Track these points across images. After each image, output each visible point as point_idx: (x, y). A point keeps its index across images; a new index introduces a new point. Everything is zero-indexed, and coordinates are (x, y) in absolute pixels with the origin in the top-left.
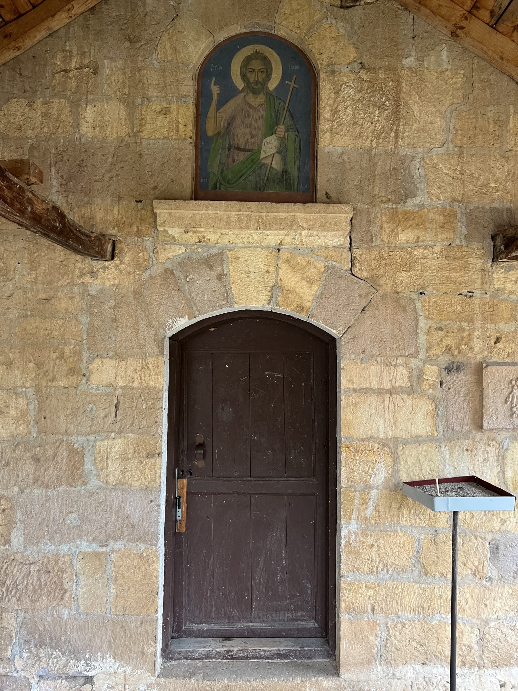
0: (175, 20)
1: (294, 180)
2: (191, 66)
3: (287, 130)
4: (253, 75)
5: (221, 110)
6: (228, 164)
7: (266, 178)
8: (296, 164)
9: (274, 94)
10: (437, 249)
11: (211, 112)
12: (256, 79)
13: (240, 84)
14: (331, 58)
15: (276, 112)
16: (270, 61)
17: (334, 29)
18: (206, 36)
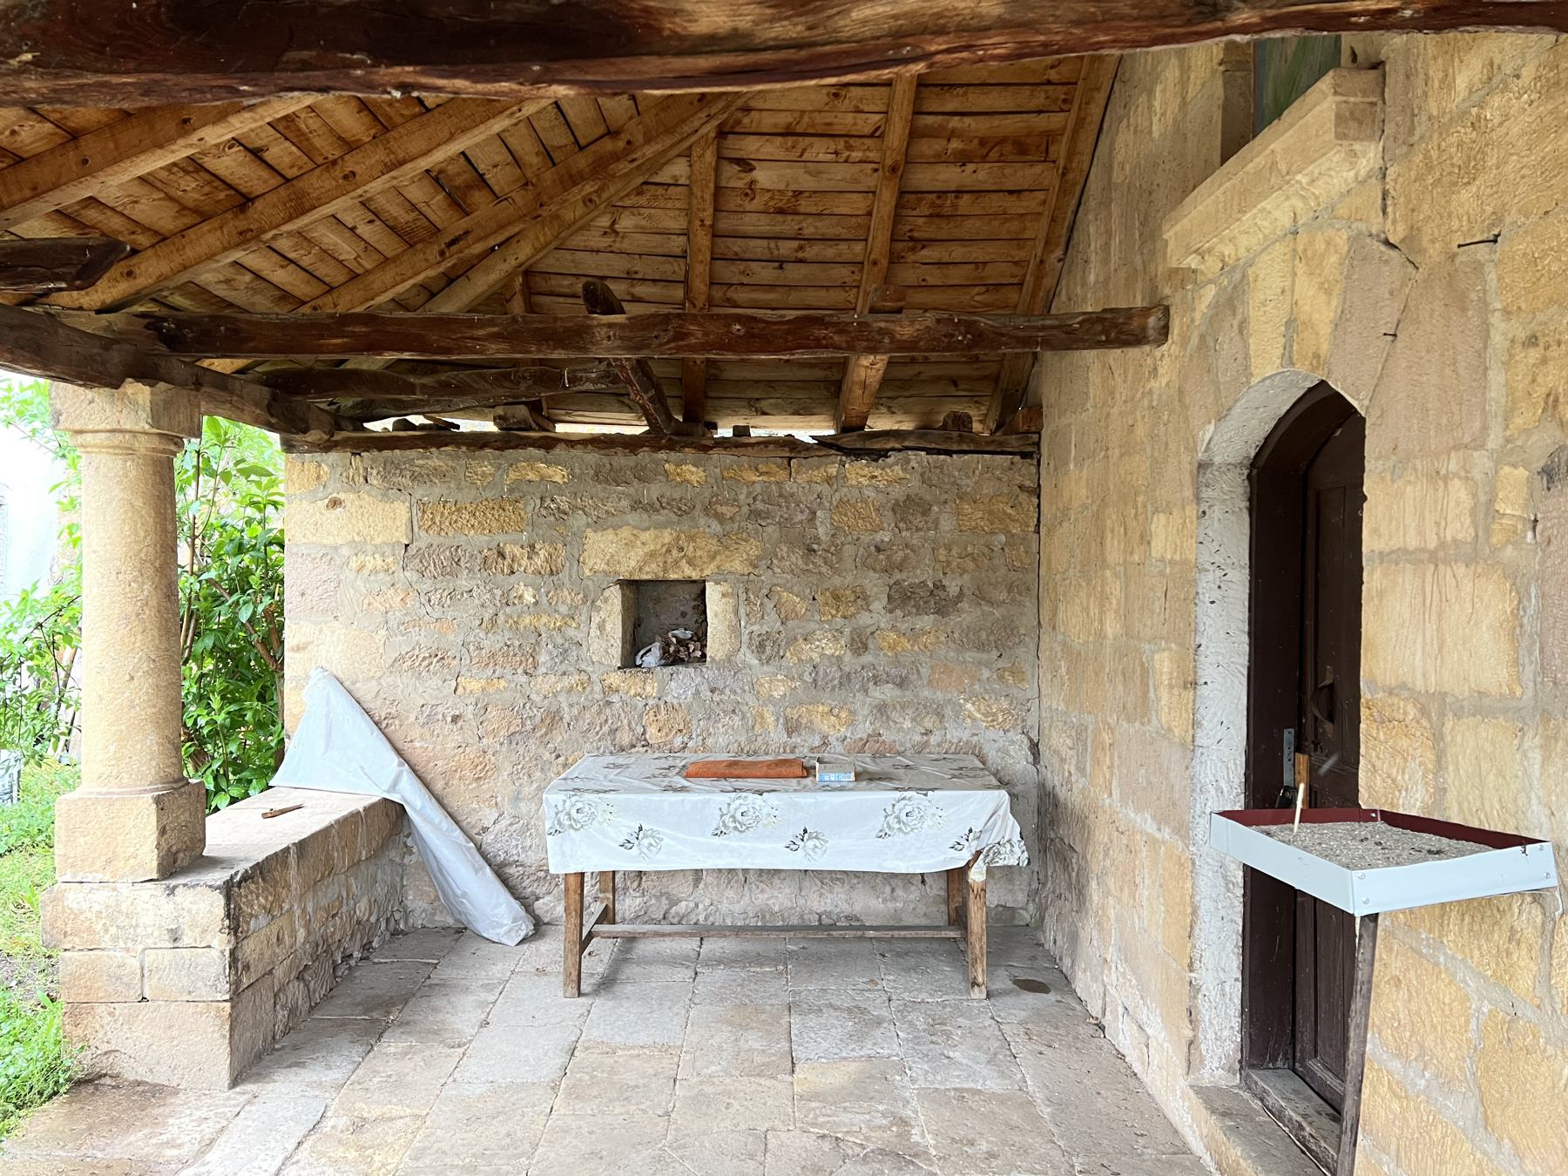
10: (1528, 73)
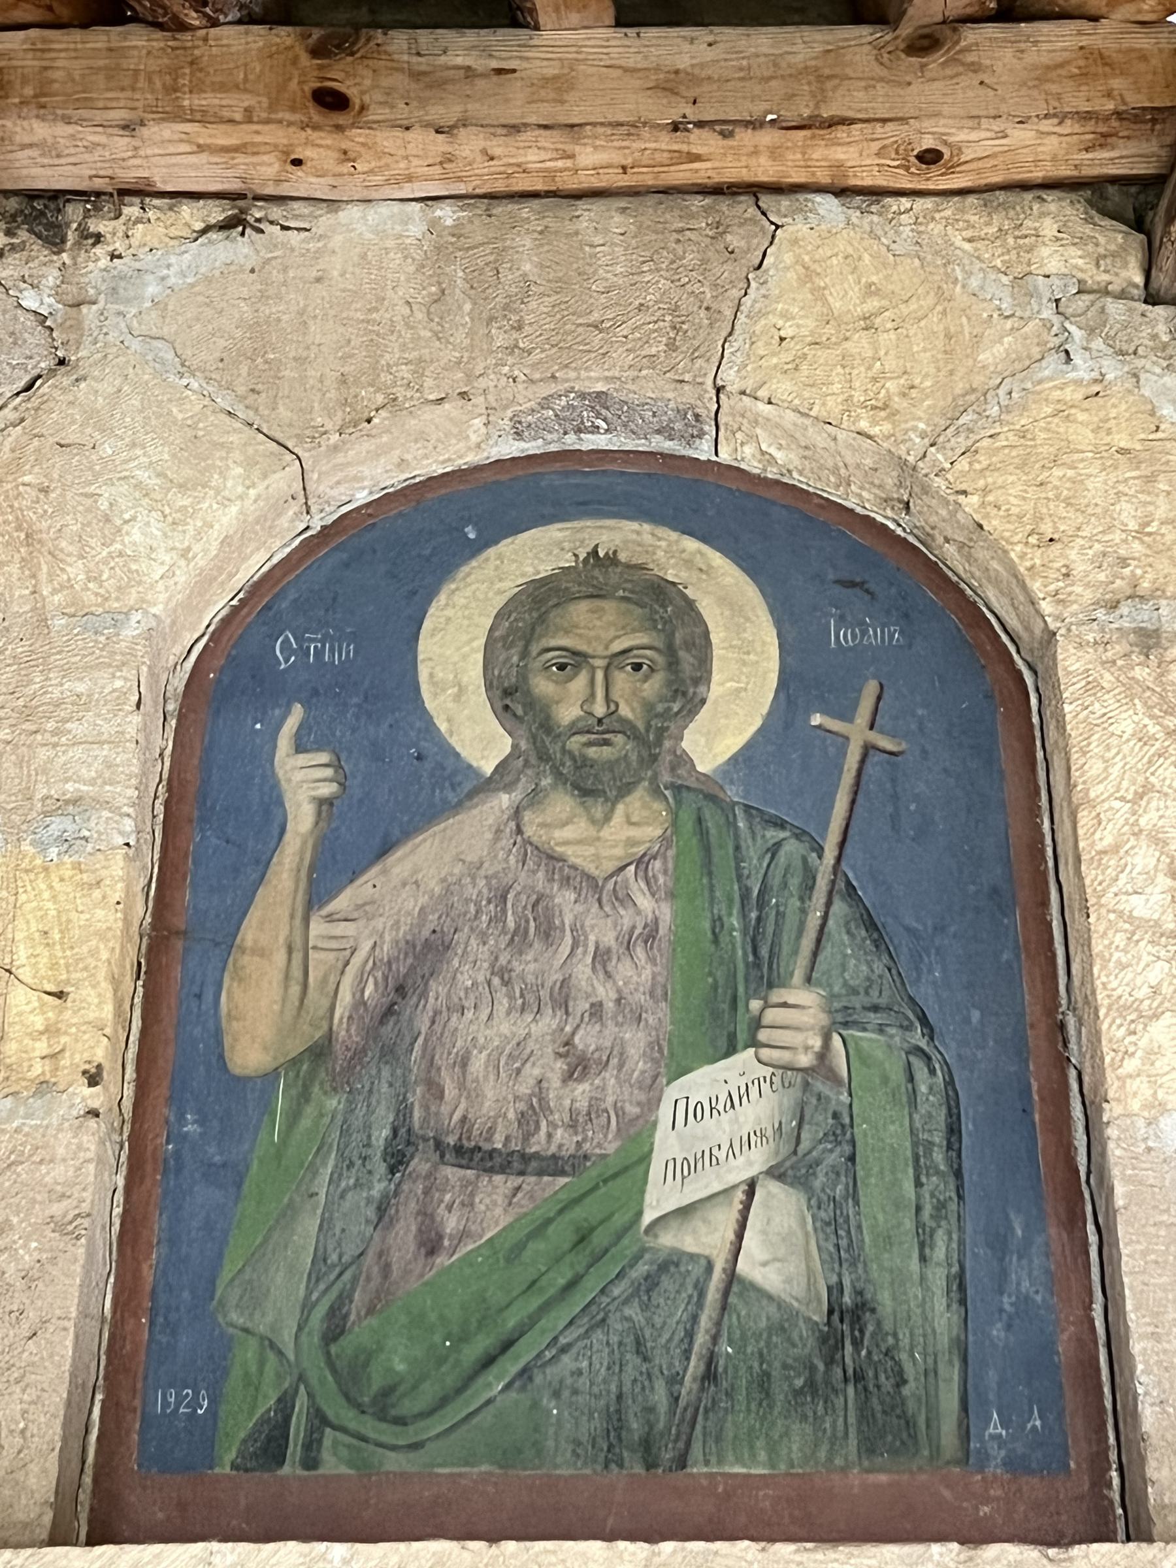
0: (43, 388)
1: (931, 1373)
2: (131, 631)
3: (842, 1019)
4: (579, 683)
5: (342, 903)
6: (386, 1270)
7: (695, 1366)
8: (939, 1252)
9: (733, 793)
11: (270, 916)
12: (600, 710)
13: (480, 738)
14: (1123, 562)
15: (756, 901)
16: (690, 604)
17: (1118, 407)
18: (250, 463)
